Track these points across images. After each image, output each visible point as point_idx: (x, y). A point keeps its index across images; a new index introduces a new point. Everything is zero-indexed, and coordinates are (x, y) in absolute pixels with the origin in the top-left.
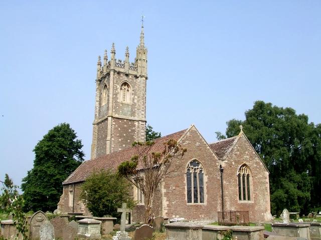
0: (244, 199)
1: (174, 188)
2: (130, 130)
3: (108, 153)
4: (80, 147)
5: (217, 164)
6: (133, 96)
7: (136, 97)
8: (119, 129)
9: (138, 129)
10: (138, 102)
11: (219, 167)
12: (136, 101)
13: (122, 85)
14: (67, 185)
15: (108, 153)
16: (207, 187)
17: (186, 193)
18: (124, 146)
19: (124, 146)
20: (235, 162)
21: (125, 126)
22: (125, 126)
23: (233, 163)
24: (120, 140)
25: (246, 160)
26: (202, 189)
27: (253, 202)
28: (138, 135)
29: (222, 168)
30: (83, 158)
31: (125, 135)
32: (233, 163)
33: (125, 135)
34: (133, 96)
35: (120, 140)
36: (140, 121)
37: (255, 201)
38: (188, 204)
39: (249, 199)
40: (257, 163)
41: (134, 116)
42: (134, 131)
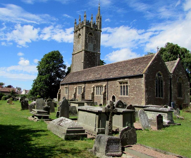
1: (150, 88)
7: (96, 41)
13: (89, 34)
16: (165, 89)
17: (155, 91)
18: (90, 65)
21: (90, 55)
22: (90, 55)
24: (88, 62)
26: (162, 89)
33: (90, 60)
35: (88, 62)
40: (185, 77)
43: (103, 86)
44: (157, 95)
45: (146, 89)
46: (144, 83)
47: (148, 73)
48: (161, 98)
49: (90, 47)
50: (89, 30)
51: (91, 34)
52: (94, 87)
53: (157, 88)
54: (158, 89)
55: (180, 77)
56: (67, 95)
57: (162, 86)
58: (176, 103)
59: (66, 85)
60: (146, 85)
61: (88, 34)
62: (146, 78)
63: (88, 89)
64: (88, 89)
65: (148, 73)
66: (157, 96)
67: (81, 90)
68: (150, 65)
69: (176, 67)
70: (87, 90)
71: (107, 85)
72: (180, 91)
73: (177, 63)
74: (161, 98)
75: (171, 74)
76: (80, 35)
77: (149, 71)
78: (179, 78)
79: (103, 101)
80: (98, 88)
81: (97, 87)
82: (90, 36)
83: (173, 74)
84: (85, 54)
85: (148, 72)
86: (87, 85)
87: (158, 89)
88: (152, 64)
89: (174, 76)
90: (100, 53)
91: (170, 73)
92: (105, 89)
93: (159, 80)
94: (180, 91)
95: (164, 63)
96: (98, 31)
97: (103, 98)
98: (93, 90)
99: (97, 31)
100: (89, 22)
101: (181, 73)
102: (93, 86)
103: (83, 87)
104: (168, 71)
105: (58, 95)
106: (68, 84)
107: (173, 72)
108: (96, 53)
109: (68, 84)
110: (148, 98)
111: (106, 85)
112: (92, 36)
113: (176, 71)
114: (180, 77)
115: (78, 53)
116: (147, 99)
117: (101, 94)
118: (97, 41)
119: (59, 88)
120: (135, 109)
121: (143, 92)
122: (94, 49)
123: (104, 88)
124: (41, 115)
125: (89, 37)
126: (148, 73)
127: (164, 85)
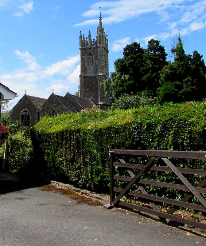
20: (47, 108)
23: (46, 109)
25: (54, 107)
32: (46, 109)
35: (87, 89)
49: (90, 70)
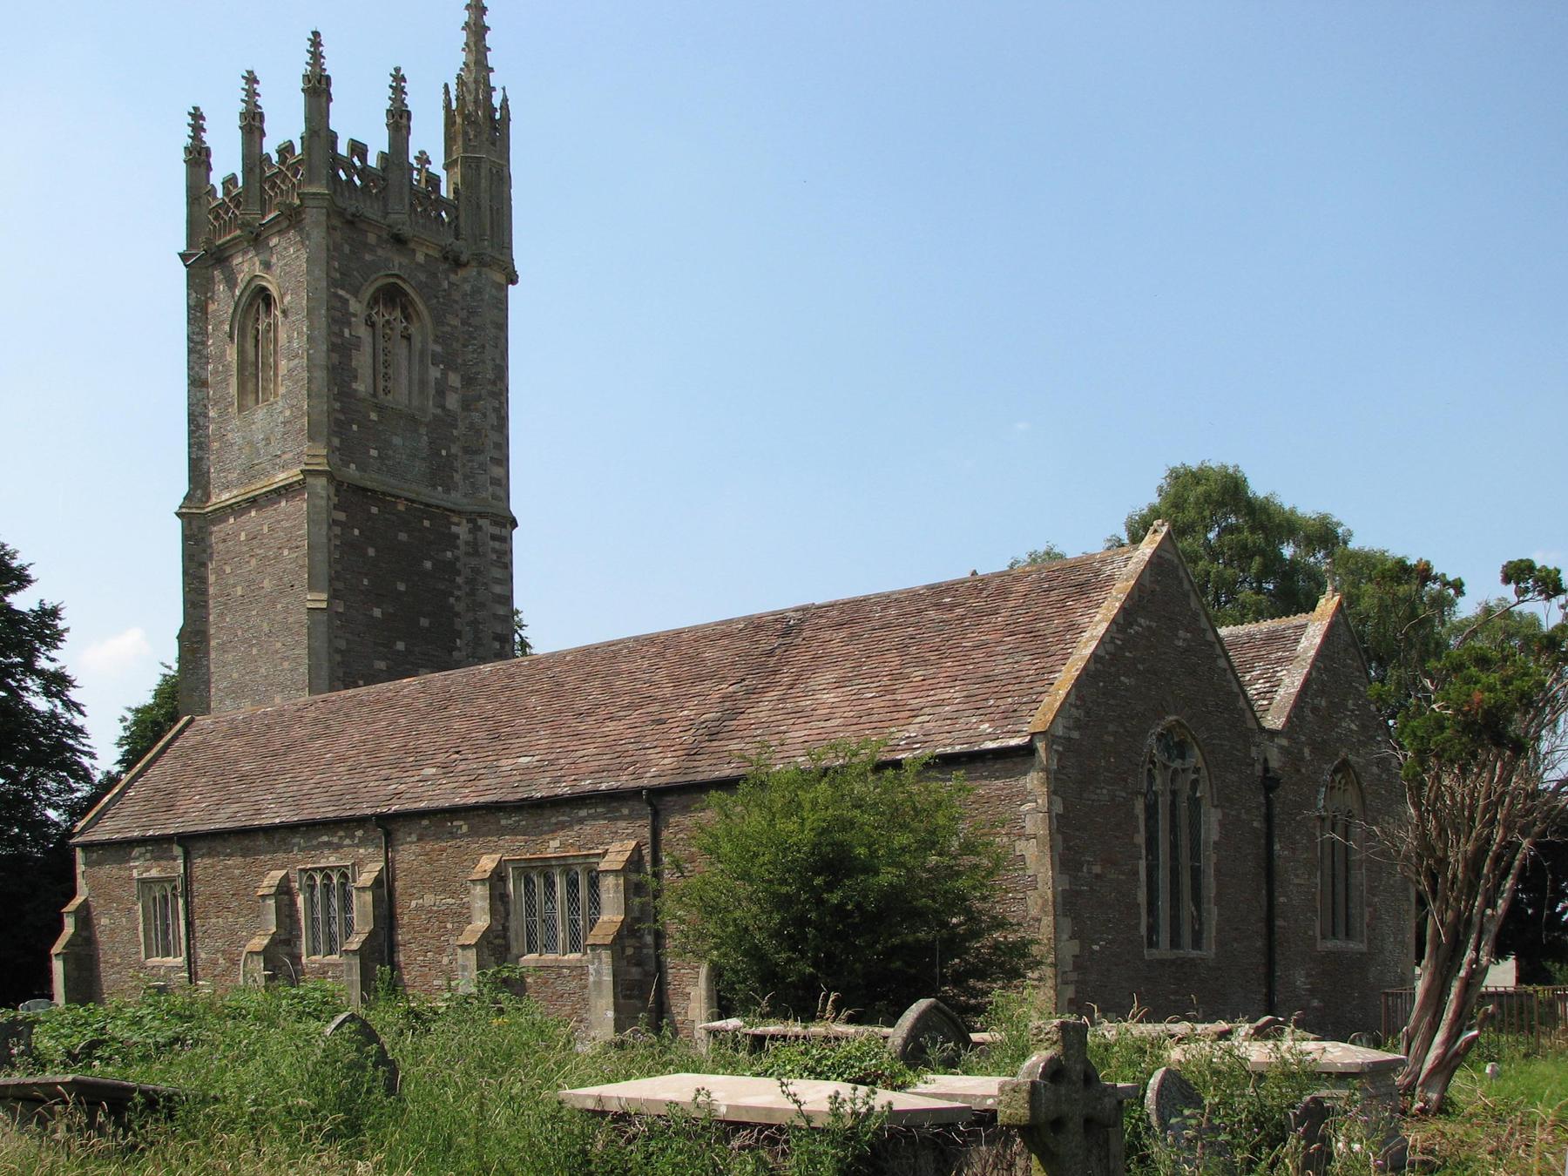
0: (1348, 935)
1: (1097, 869)
2: (428, 565)
3: (1223, 631)
4: (54, 638)
5: (1254, 752)
6: (435, 373)
7: (454, 379)
8: (371, 552)
9: (474, 562)
10: (466, 405)
11: (1258, 768)
12: (452, 402)
13: (374, 301)
14: (120, 849)
15: (1223, 631)
16: (1218, 870)
17: (1142, 897)
18: (400, 646)
19: (400, 646)
22: (403, 536)
23: (1307, 751)
24: (377, 612)
26: (1196, 874)
27: (1363, 947)
28: (472, 593)
29: (1271, 774)
30: (73, 694)
31: (402, 587)
33: (402, 587)
34: (435, 373)
35: (377, 612)
36: (481, 515)
37: (1370, 941)
38: (1147, 953)
39: (1197, 943)
41: (447, 490)
42: (451, 568)
43: (603, 866)
44: (1153, 929)
45: (1066, 878)
46: (1043, 831)
47: (1075, 735)
48: (1194, 953)
50: (372, 250)
51: (391, 296)
52: (497, 879)
53: (1152, 871)
54: (1163, 876)
55: (1345, 763)
56: (180, 960)
57: (1195, 854)
58: (1312, 992)
59: (156, 859)
60: (1060, 847)
61: (355, 293)
62: (1057, 784)
63: (429, 899)
64: (429, 899)
65: (1075, 735)
66: (1152, 944)
67: (335, 903)
68: (1094, 656)
69: (1309, 673)
70: (413, 904)
71: (646, 851)
72: (1340, 887)
73: (1318, 640)
74: (1194, 953)
75: (1273, 734)
76: (262, 298)
77: (1087, 713)
78: (1336, 771)
79: (611, 1014)
80: (539, 882)
81: (529, 881)
82: (382, 316)
83: (1284, 742)
84: (341, 516)
85: (1078, 720)
86: (409, 854)
87: (1163, 876)
88: (1110, 648)
89: (1292, 757)
90: (208, 145)
91: (1262, 729)
92: (634, 889)
93: (1169, 798)
94: (1340, 887)
95: (1210, 637)
96: (471, 272)
97: (608, 979)
98: (486, 905)
99: (462, 273)
100: (363, 158)
101: (1353, 727)
102: (488, 863)
103: (366, 877)
104: (1249, 715)
105: (58, 967)
106: (178, 850)
107: (1289, 718)
108: (459, 513)
109: (168, 839)
110: (1077, 967)
111: (638, 848)
112: (407, 318)
113: (1315, 710)
114: (1345, 763)
115: (253, 502)
116: (1073, 976)
117: (594, 947)
118: (468, 381)
119: (72, 894)
120: (367, 237)
121: (1034, 912)
122: (440, 473)
123: (611, 891)
124: (304, 930)
125: (379, 332)
126: (1078, 728)
127: (1215, 837)
